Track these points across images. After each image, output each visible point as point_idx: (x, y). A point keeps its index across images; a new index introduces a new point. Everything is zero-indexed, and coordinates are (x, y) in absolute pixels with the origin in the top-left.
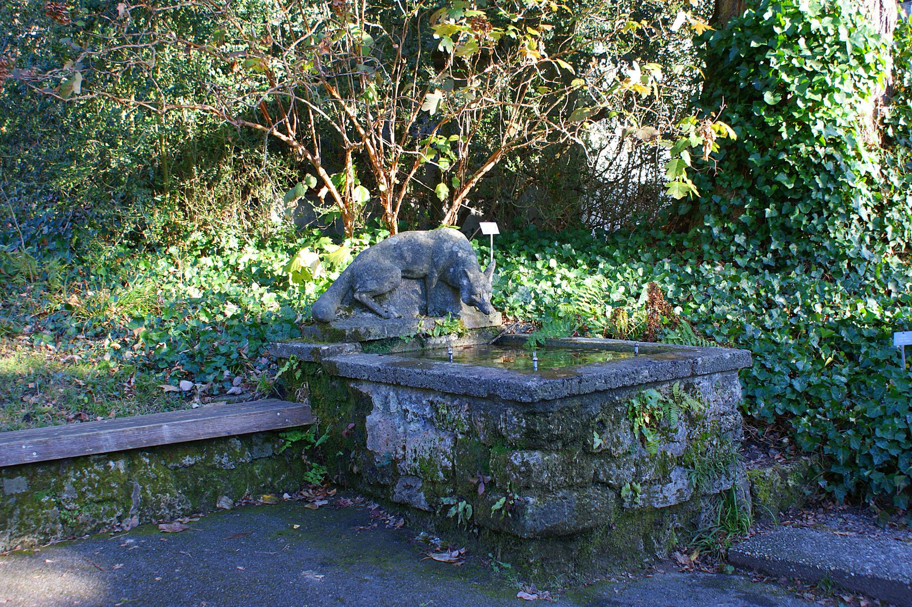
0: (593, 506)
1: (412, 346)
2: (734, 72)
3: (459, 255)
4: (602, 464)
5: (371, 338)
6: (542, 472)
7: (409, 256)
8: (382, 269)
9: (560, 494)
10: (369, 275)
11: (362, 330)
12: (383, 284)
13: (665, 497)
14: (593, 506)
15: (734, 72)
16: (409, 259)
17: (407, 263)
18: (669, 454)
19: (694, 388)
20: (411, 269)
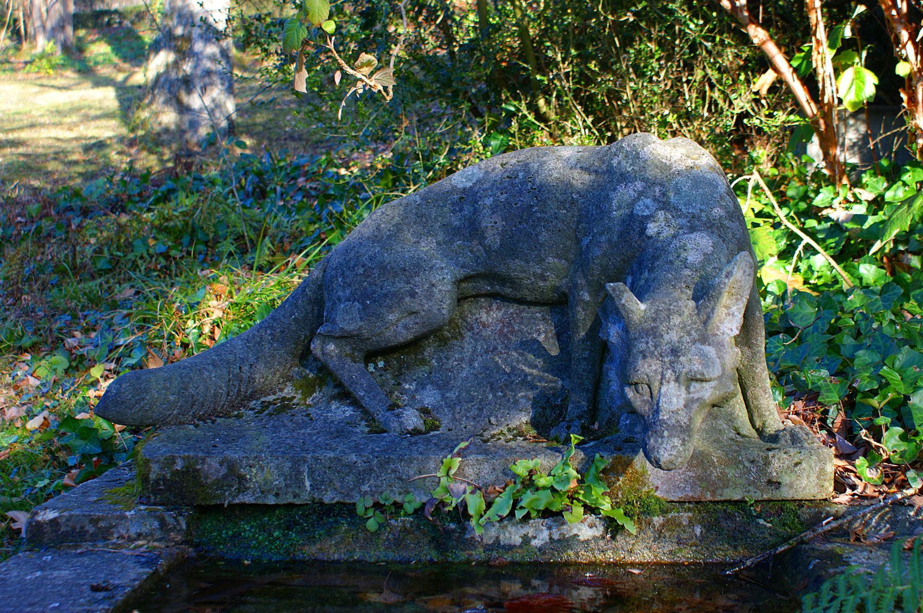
1: (398, 543)
2: (31, 2)
3: (652, 229)
5: (248, 499)
7: (493, 227)
8: (383, 268)
11: (213, 467)
12: (379, 317)
15: (31, 2)
17: (488, 250)
20: (502, 269)
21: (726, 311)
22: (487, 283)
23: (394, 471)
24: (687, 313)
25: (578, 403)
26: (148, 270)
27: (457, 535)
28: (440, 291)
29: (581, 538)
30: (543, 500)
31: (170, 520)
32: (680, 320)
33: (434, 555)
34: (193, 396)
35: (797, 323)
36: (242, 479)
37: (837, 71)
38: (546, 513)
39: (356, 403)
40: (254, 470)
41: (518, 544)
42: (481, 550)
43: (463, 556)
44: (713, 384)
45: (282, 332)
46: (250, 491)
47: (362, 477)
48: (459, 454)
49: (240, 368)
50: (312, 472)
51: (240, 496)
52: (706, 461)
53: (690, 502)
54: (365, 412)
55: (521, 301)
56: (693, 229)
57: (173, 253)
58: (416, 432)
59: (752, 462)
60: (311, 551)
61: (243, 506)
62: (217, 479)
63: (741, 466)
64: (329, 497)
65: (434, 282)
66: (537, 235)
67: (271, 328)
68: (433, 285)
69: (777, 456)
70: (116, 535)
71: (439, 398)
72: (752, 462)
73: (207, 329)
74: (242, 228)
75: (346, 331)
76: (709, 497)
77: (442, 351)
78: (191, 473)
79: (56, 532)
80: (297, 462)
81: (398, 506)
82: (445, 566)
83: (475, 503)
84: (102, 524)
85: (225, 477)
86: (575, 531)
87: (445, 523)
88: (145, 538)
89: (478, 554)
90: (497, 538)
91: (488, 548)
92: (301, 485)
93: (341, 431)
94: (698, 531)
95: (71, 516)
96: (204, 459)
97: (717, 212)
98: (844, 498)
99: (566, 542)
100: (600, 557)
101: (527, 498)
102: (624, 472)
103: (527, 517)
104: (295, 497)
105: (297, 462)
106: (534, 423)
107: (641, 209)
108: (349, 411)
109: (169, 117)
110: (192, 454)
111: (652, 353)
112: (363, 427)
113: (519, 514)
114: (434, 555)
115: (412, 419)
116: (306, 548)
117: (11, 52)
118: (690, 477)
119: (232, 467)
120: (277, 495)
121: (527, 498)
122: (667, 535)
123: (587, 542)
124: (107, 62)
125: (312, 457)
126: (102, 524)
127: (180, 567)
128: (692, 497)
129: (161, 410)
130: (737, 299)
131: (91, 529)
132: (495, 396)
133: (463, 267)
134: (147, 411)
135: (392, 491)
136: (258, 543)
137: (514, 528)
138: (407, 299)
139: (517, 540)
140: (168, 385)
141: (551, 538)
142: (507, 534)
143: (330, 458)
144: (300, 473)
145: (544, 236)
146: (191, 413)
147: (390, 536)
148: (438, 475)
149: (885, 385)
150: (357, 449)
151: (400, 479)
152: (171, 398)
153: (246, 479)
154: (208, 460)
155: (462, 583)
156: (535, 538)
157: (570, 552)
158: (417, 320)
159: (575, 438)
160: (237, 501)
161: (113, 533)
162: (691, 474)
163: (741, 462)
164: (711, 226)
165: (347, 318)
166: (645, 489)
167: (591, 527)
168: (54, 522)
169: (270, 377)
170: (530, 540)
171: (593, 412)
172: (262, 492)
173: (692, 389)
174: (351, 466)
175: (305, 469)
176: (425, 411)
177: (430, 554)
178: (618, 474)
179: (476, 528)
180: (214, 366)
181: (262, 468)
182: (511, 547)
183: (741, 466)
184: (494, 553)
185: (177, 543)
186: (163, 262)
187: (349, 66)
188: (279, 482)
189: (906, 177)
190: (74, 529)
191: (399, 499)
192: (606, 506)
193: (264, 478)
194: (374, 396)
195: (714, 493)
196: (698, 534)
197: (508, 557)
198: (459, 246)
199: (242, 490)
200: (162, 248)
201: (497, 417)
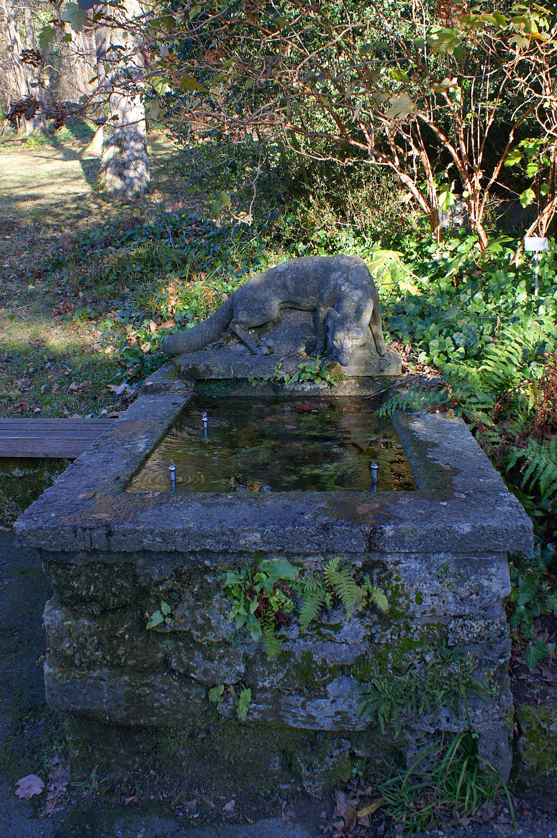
0: (157, 700)
1: (262, 390)
3: (343, 288)
4: (178, 648)
5: (213, 377)
6: (62, 639)
8: (254, 300)
9: (97, 673)
10: (241, 305)
13: (310, 716)
14: (157, 700)
16: (291, 290)
18: (316, 658)
19: (385, 569)
22: (291, 305)
25: (320, 344)
26: (134, 279)
30: (308, 376)
33: (274, 394)
35: (407, 310)
36: (211, 370)
37: (438, 193)
38: (309, 380)
39: (245, 345)
43: (283, 394)
47: (250, 370)
54: (249, 348)
55: (301, 310)
56: (356, 289)
57: (145, 271)
58: (266, 355)
60: (234, 393)
73: (170, 309)
74: (176, 259)
78: (194, 369)
80: (229, 365)
81: (262, 379)
82: (278, 397)
83: (286, 377)
87: (277, 384)
89: (288, 394)
91: (291, 391)
93: (241, 355)
97: (365, 282)
98: (405, 375)
99: (317, 389)
101: (303, 375)
103: (303, 382)
105: (229, 365)
106: (306, 351)
107: (339, 282)
108: (243, 348)
109: (118, 184)
112: (248, 353)
113: (301, 381)
114: (274, 394)
115: (265, 350)
117: (12, 133)
119: (208, 367)
121: (303, 375)
124: (67, 139)
127: (194, 399)
136: (216, 391)
149: (424, 337)
150: (248, 360)
155: (282, 402)
159: (318, 356)
164: (363, 288)
165: (243, 317)
171: (325, 347)
174: (246, 366)
176: (269, 347)
177: (272, 393)
179: (287, 385)
186: (140, 275)
189: (467, 240)
192: (328, 378)
193: (218, 370)
197: (297, 394)
200: (139, 269)
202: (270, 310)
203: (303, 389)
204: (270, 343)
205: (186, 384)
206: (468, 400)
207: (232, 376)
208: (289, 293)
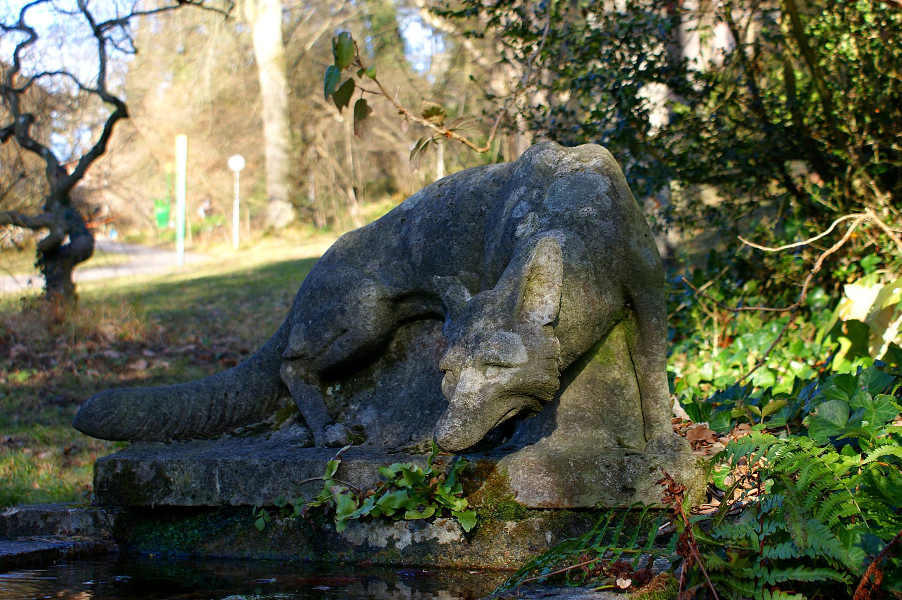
1: (282, 543)
5: (171, 501)
11: (145, 471)
21: (540, 300)
23: (289, 474)
24: (500, 301)
27: (331, 535)
28: (365, 307)
29: (441, 542)
31: (101, 517)
32: (491, 308)
33: (311, 556)
34: (165, 415)
36: (167, 480)
40: (176, 473)
41: (384, 546)
42: (352, 551)
43: (336, 556)
44: (514, 370)
45: (269, 361)
46: (173, 494)
48: (339, 457)
49: (226, 395)
50: (222, 475)
51: (165, 499)
52: (563, 466)
53: (548, 509)
59: (608, 467)
61: (167, 507)
62: (148, 482)
63: (597, 472)
64: (235, 500)
65: (360, 298)
66: (449, 249)
67: (260, 357)
68: (359, 302)
69: (632, 461)
70: (60, 531)
71: (375, 416)
72: (608, 467)
75: (294, 352)
76: (566, 504)
77: (388, 372)
79: (15, 526)
81: (290, 508)
84: (50, 520)
85: (154, 479)
86: (435, 535)
88: (82, 534)
89: (349, 555)
90: (366, 539)
91: (359, 549)
92: (213, 489)
94: (549, 536)
95: (27, 512)
96: (138, 463)
100: (457, 561)
102: (487, 477)
104: (208, 499)
110: (129, 458)
111: (460, 340)
114: (311, 556)
116: (206, 545)
118: (548, 482)
119: (160, 470)
120: (194, 497)
122: (520, 540)
123: (446, 545)
125: (223, 461)
126: (50, 520)
128: (550, 503)
129: (130, 425)
130: (550, 287)
131: (41, 524)
132: (422, 414)
133: (395, 286)
134: (116, 425)
135: (287, 494)
137: (381, 530)
138: (339, 317)
139: (383, 542)
140: (139, 402)
141: (413, 541)
142: (374, 536)
143: (237, 462)
144: (212, 476)
145: (456, 249)
146: (163, 431)
147: (276, 536)
148: (324, 478)
151: (293, 482)
152: (141, 414)
153: (170, 482)
154: (141, 463)
156: (399, 540)
157: (431, 557)
158: (348, 338)
160: (162, 503)
161: (57, 528)
162: (548, 479)
163: (597, 467)
166: (507, 495)
167: (449, 530)
168: (14, 516)
169: (258, 405)
170: (395, 543)
172: (183, 495)
173: (488, 374)
174: (253, 469)
175: (216, 472)
178: (483, 479)
180: (197, 390)
181: (182, 471)
182: (378, 549)
183: (597, 472)
184: (363, 554)
185: (105, 538)
187: (255, 88)
188: (196, 485)
190: (29, 523)
191: (292, 502)
194: (316, 414)
195: (571, 500)
196: (549, 540)
197: (374, 559)
198: (395, 265)
199: (168, 492)
201: (418, 434)
202: (356, 313)
203: (391, 541)
204: (367, 418)
205: (95, 517)
206: (769, 553)
207: (216, 500)
208: (413, 265)
